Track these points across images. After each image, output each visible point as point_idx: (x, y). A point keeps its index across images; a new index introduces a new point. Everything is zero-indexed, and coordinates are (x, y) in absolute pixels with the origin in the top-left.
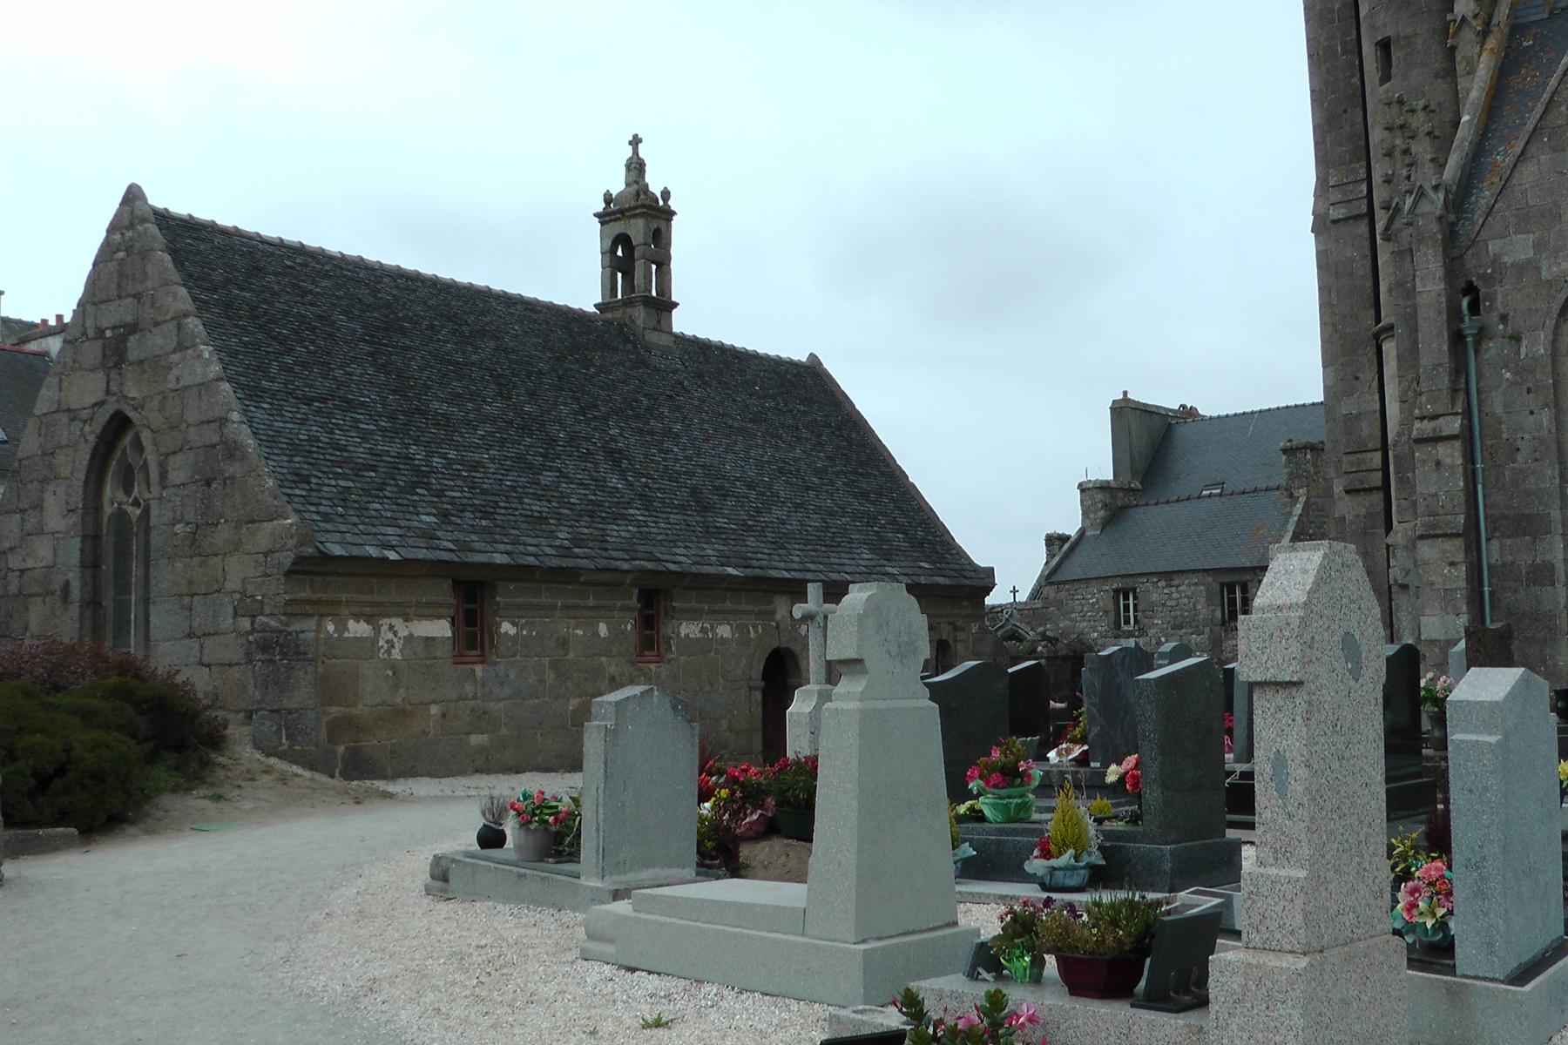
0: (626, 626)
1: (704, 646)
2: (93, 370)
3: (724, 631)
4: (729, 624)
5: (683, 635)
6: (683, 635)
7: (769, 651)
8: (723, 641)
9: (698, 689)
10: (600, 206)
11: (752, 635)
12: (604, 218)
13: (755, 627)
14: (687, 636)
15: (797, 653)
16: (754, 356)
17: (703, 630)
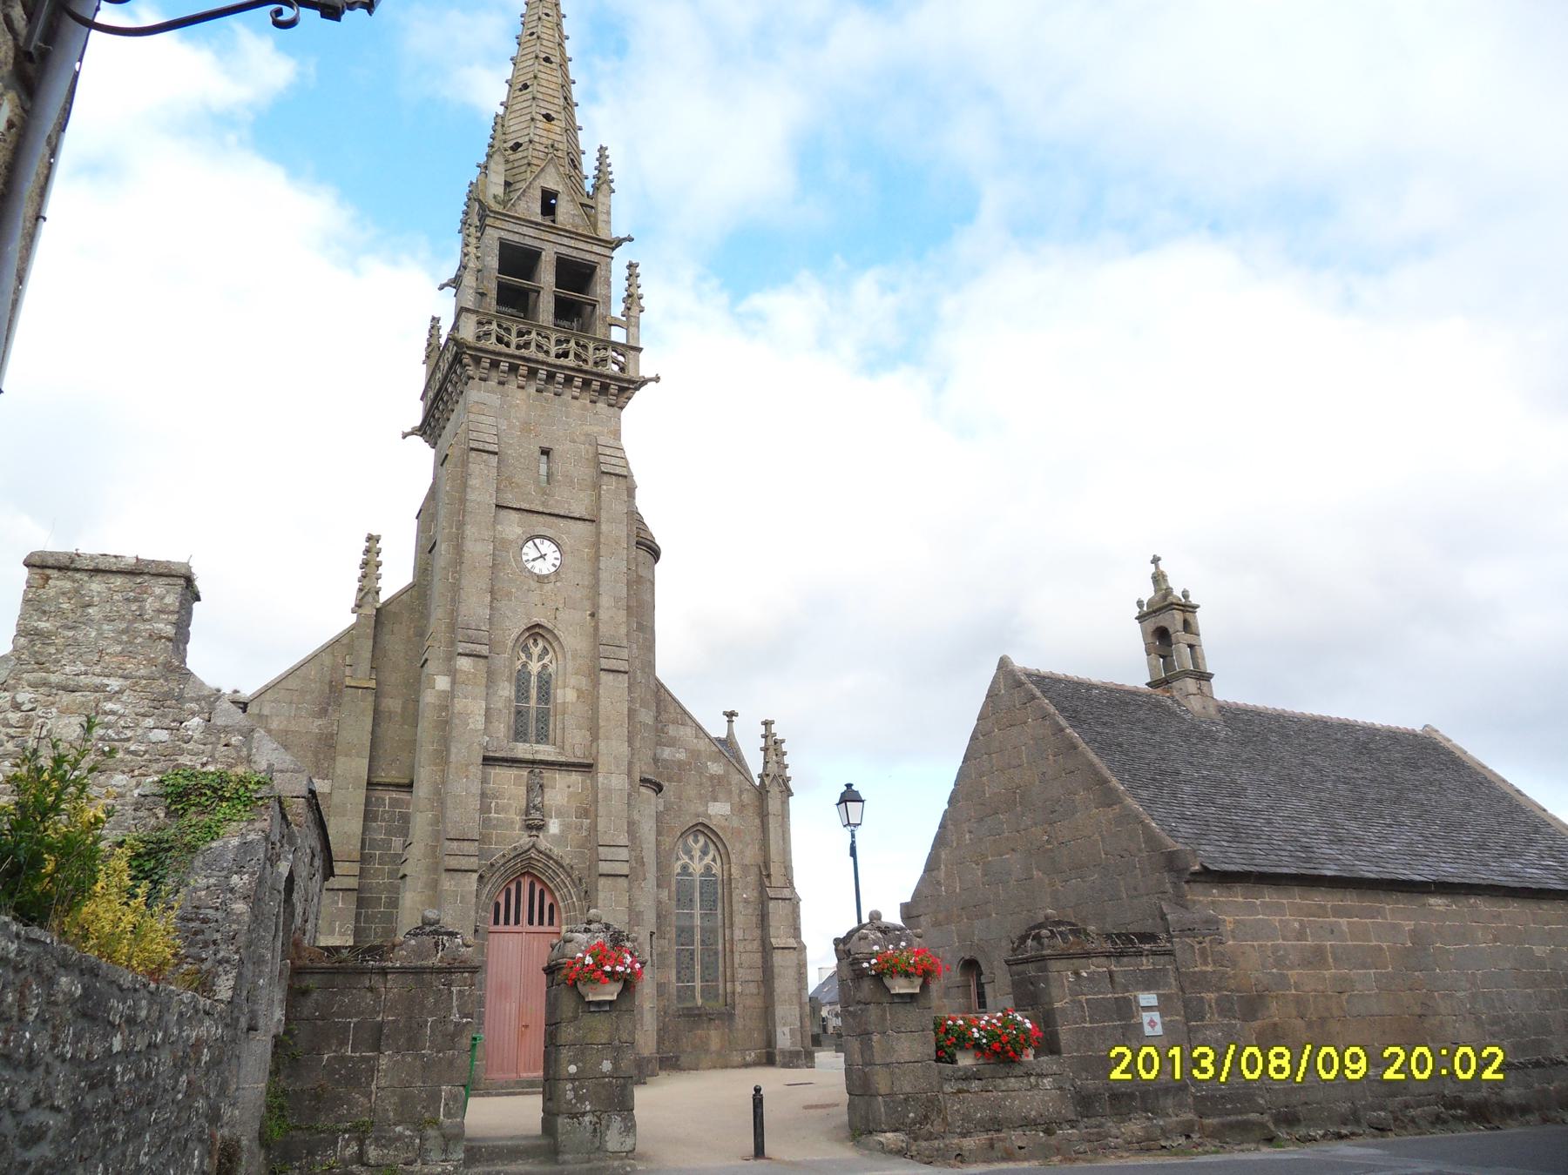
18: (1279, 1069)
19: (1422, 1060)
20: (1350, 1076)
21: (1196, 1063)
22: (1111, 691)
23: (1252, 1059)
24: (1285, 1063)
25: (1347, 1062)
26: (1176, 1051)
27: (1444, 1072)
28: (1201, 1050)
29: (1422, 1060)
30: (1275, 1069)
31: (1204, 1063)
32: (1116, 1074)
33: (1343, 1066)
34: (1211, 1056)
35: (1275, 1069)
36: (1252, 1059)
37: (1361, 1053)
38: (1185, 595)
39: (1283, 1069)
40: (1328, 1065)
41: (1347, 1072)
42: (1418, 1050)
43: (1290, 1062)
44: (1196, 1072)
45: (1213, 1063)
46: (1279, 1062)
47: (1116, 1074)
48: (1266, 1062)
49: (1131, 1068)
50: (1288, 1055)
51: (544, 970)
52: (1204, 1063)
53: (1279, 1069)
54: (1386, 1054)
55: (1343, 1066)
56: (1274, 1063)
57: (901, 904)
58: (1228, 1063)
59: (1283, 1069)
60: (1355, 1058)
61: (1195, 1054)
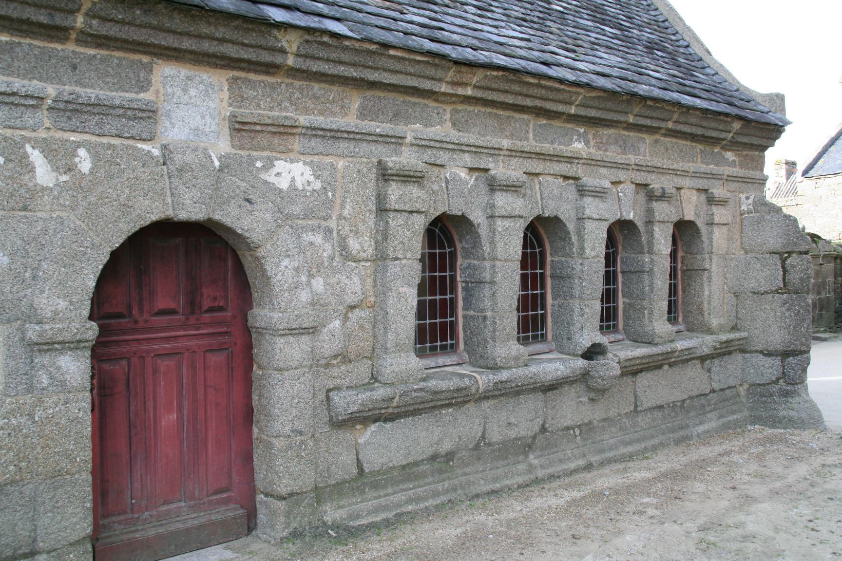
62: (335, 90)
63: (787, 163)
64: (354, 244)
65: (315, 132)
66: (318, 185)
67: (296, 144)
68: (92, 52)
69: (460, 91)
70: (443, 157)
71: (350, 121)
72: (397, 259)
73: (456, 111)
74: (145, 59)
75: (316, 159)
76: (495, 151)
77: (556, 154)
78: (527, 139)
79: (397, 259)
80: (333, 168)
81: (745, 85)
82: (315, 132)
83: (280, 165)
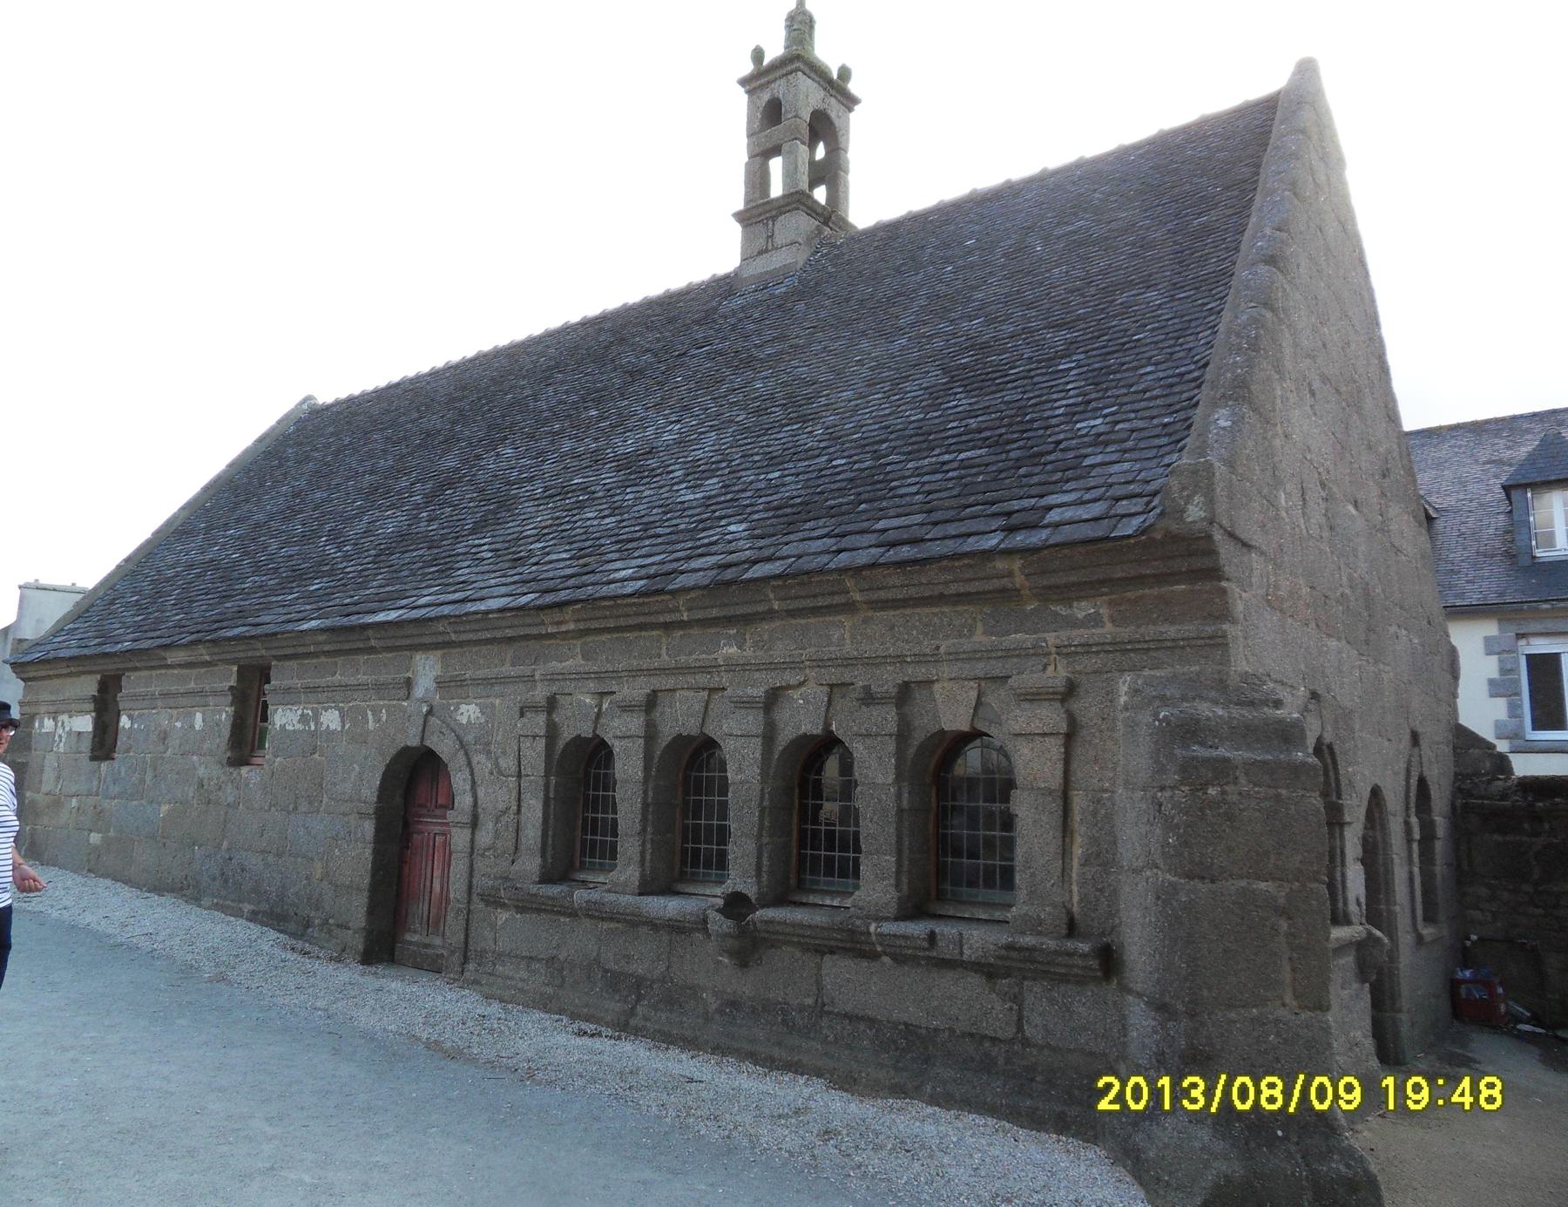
0: (221, 715)
1: (314, 741)
2: (972, 724)
3: (331, 719)
4: (337, 708)
5: (278, 727)
6: (278, 727)
7: (393, 751)
8: (330, 733)
9: (291, 808)
10: (748, 68)
11: (371, 725)
12: (752, 84)
13: (376, 712)
14: (283, 727)
15: (444, 757)
16: (1366, 275)
17: (304, 719)
18: (1272, 1100)
19: (1137, 1090)
20: (1345, 1107)
21: (1186, 1093)
22: (1349, 212)
23: (1321, 1090)
24: (1277, 1093)
25: (1341, 1092)
26: (1165, 1082)
27: (1441, 1102)
28: (1191, 1079)
29: (1137, 1090)
30: (1486, 1099)
31: (1195, 1093)
32: (1104, 1105)
33: (1336, 1097)
34: (1202, 1086)
35: (1486, 1099)
36: (1321, 1090)
37: (1356, 1083)
38: (845, 73)
39: (1495, 1099)
40: (1321, 1096)
41: (1341, 1102)
42: (1133, 1080)
43: (1501, 1092)
44: (1185, 1103)
45: (1204, 1093)
46: (1490, 1092)
47: (1104, 1105)
48: (1258, 1092)
49: (1120, 1099)
50: (1280, 1084)
51: (743, 82)
52: (1195, 1093)
53: (1272, 1100)
54: (1101, 1084)
55: (1336, 1097)
56: (1266, 1093)
57: (1492, 696)
58: (1218, 1093)
59: (1495, 1099)
60: (1349, 1088)
61: (1185, 1084)
62: (495, 648)
63: (522, 715)
64: (503, 763)
65: (476, 682)
66: (483, 721)
67: (472, 691)
68: (390, 655)
69: (564, 628)
70: (569, 687)
71: (508, 669)
72: (528, 776)
73: (585, 643)
74: (408, 653)
75: (482, 700)
76: (615, 675)
77: (679, 666)
78: (659, 656)
79: (528, 776)
80: (493, 705)
81: (1470, 420)
82: (476, 682)
83: (463, 708)
